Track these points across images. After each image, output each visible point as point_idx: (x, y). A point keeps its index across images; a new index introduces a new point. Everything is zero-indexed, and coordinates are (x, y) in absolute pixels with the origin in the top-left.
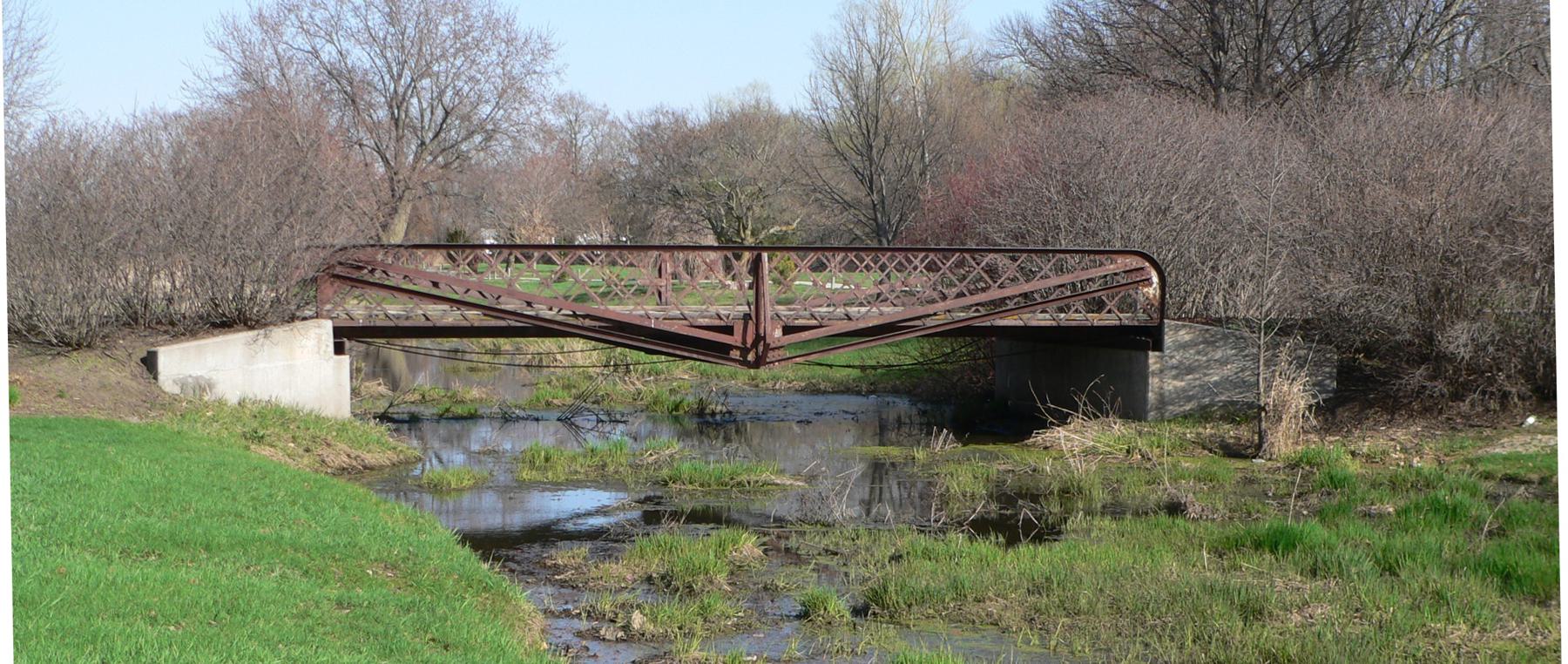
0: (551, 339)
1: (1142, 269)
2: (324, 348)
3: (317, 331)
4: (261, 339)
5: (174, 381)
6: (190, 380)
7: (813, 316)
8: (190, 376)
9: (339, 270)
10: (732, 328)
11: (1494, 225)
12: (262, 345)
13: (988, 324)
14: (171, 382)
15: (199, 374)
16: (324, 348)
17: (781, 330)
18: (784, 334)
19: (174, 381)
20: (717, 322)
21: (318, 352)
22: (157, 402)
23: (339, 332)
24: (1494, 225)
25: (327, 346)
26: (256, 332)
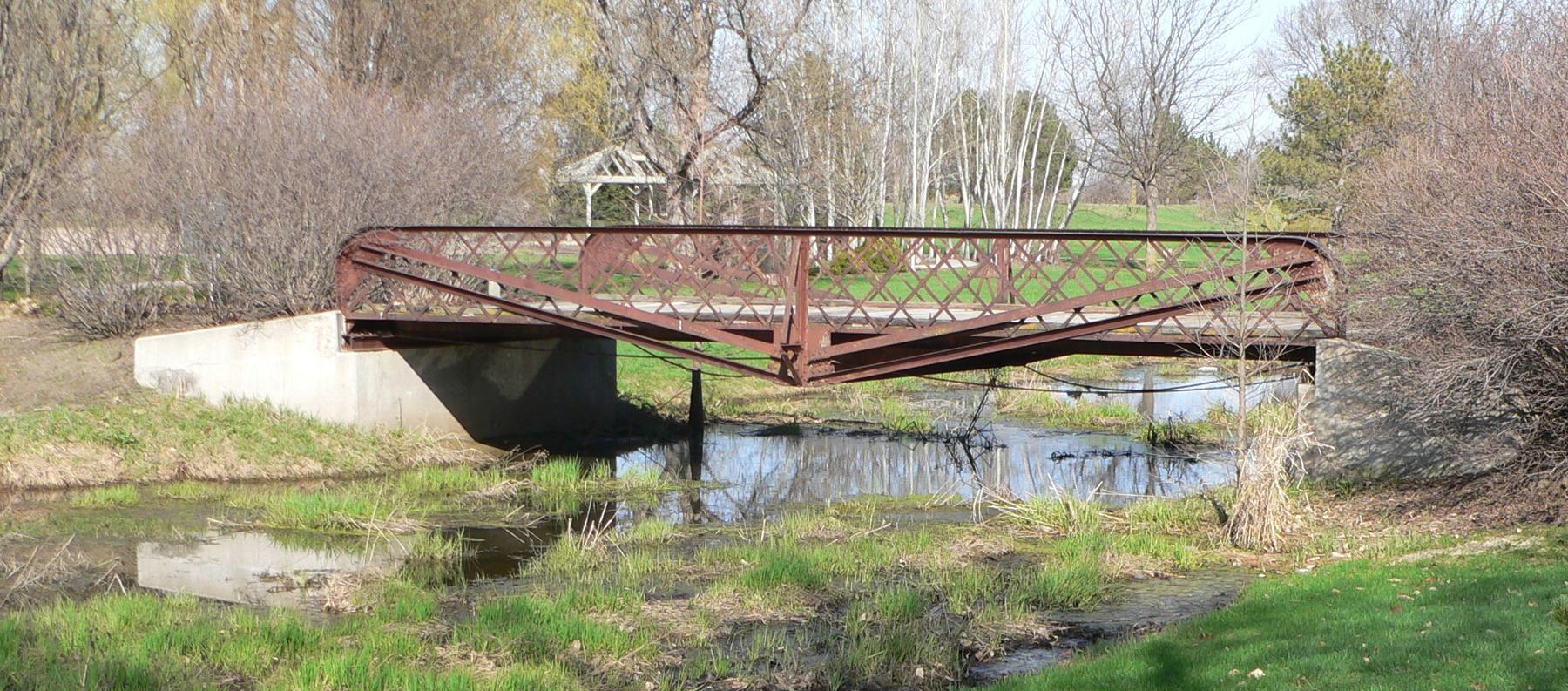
0: (1107, 357)
1: (1309, 264)
2: (324, 343)
3: (317, 323)
4: (251, 333)
5: (151, 374)
6: (169, 374)
7: (868, 320)
8: (169, 369)
9: (360, 256)
10: (771, 333)
11: (1011, 571)
12: (253, 338)
13: (1095, 338)
14: (148, 375)
15: (179, 368)
16: (324, 343)
17: (829, 337)
18: (833, 344)
19: (151, 374)
20: (754, 326)
21: (318, 348)
22: (132, 391)
23: (358, 325)
24: (1011, 571)
25: (329, 341)
26: (246, 324)
